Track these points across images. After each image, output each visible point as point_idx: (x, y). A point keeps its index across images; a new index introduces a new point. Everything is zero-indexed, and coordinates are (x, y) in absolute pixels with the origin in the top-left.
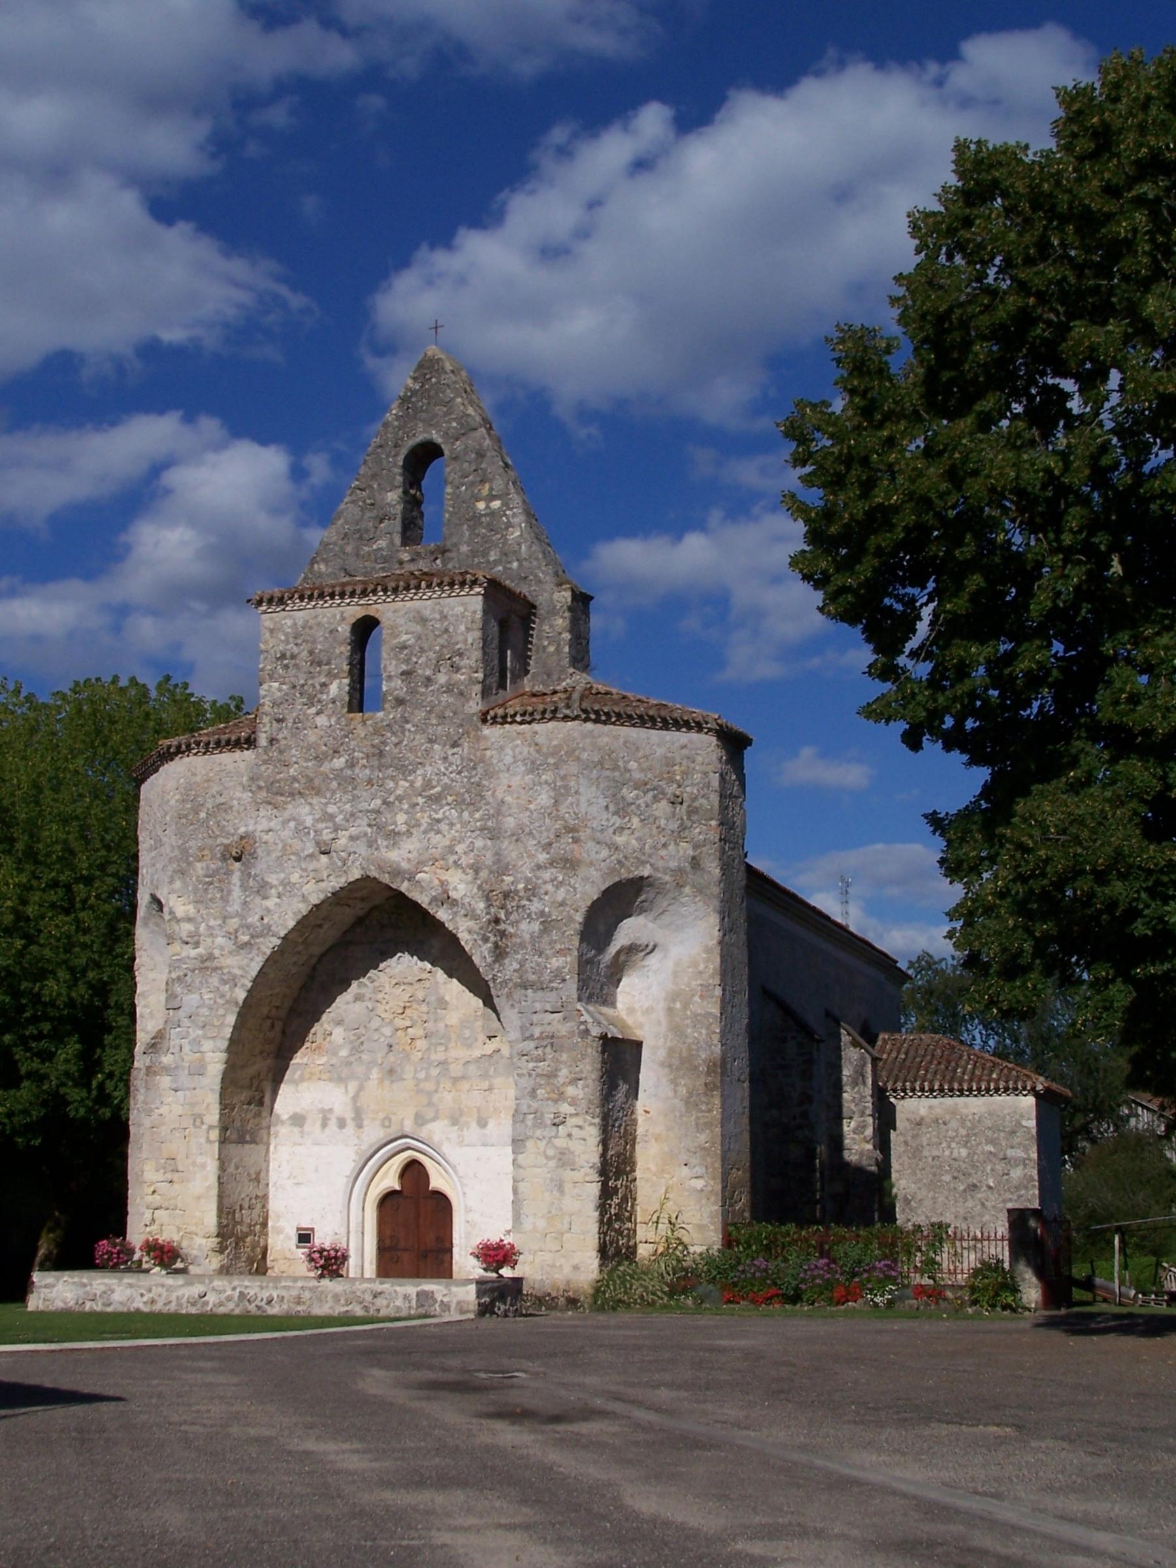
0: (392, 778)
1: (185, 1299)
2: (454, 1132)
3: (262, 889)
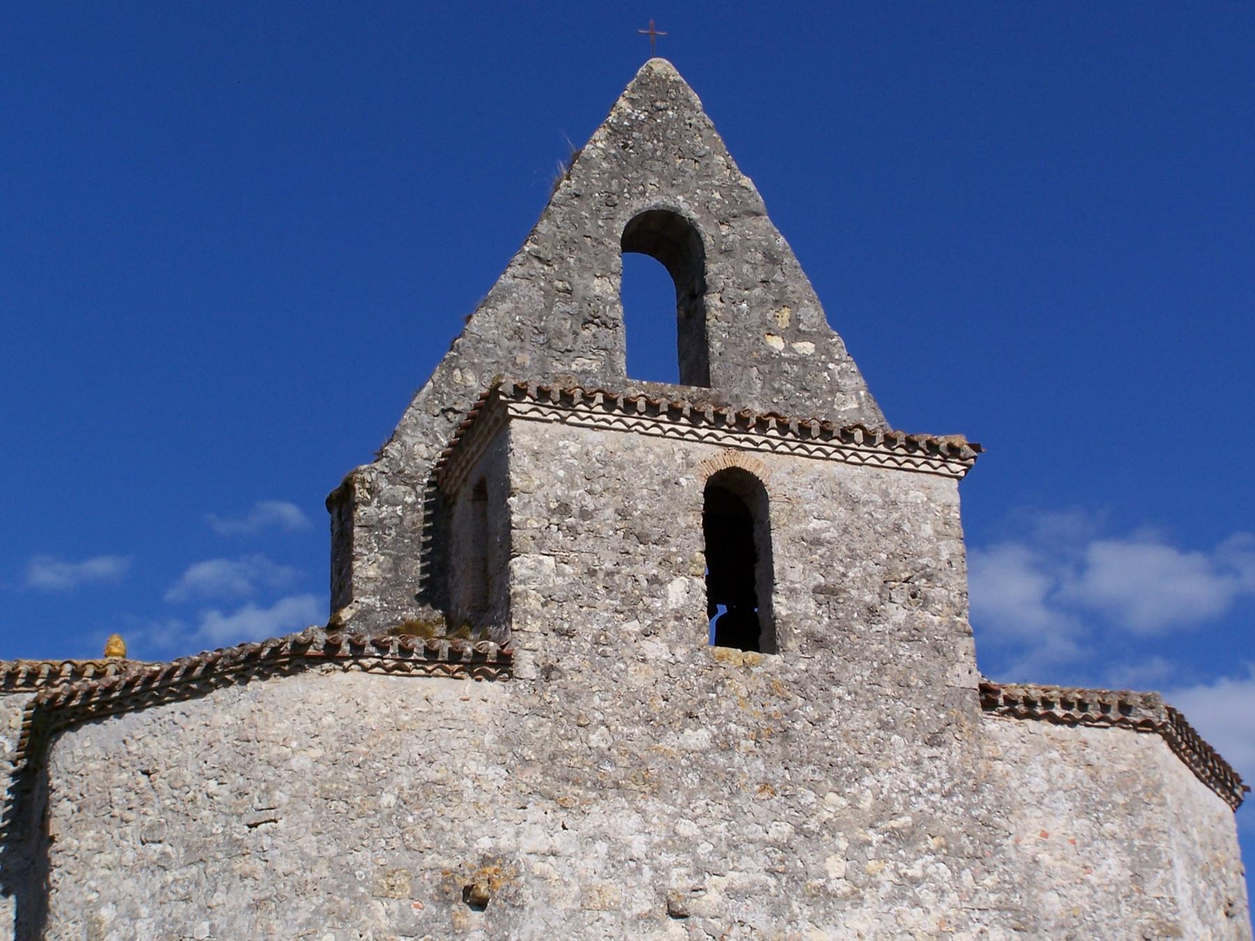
0: (813, 786)
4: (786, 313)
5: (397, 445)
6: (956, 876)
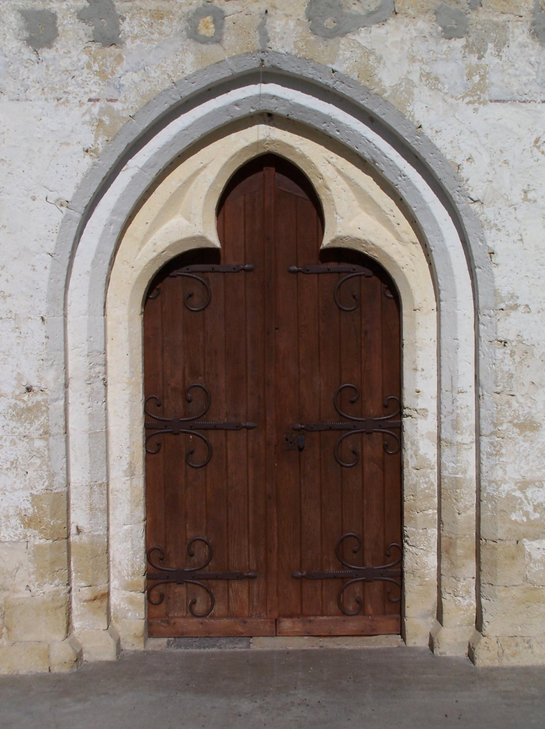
2: (451, 60)
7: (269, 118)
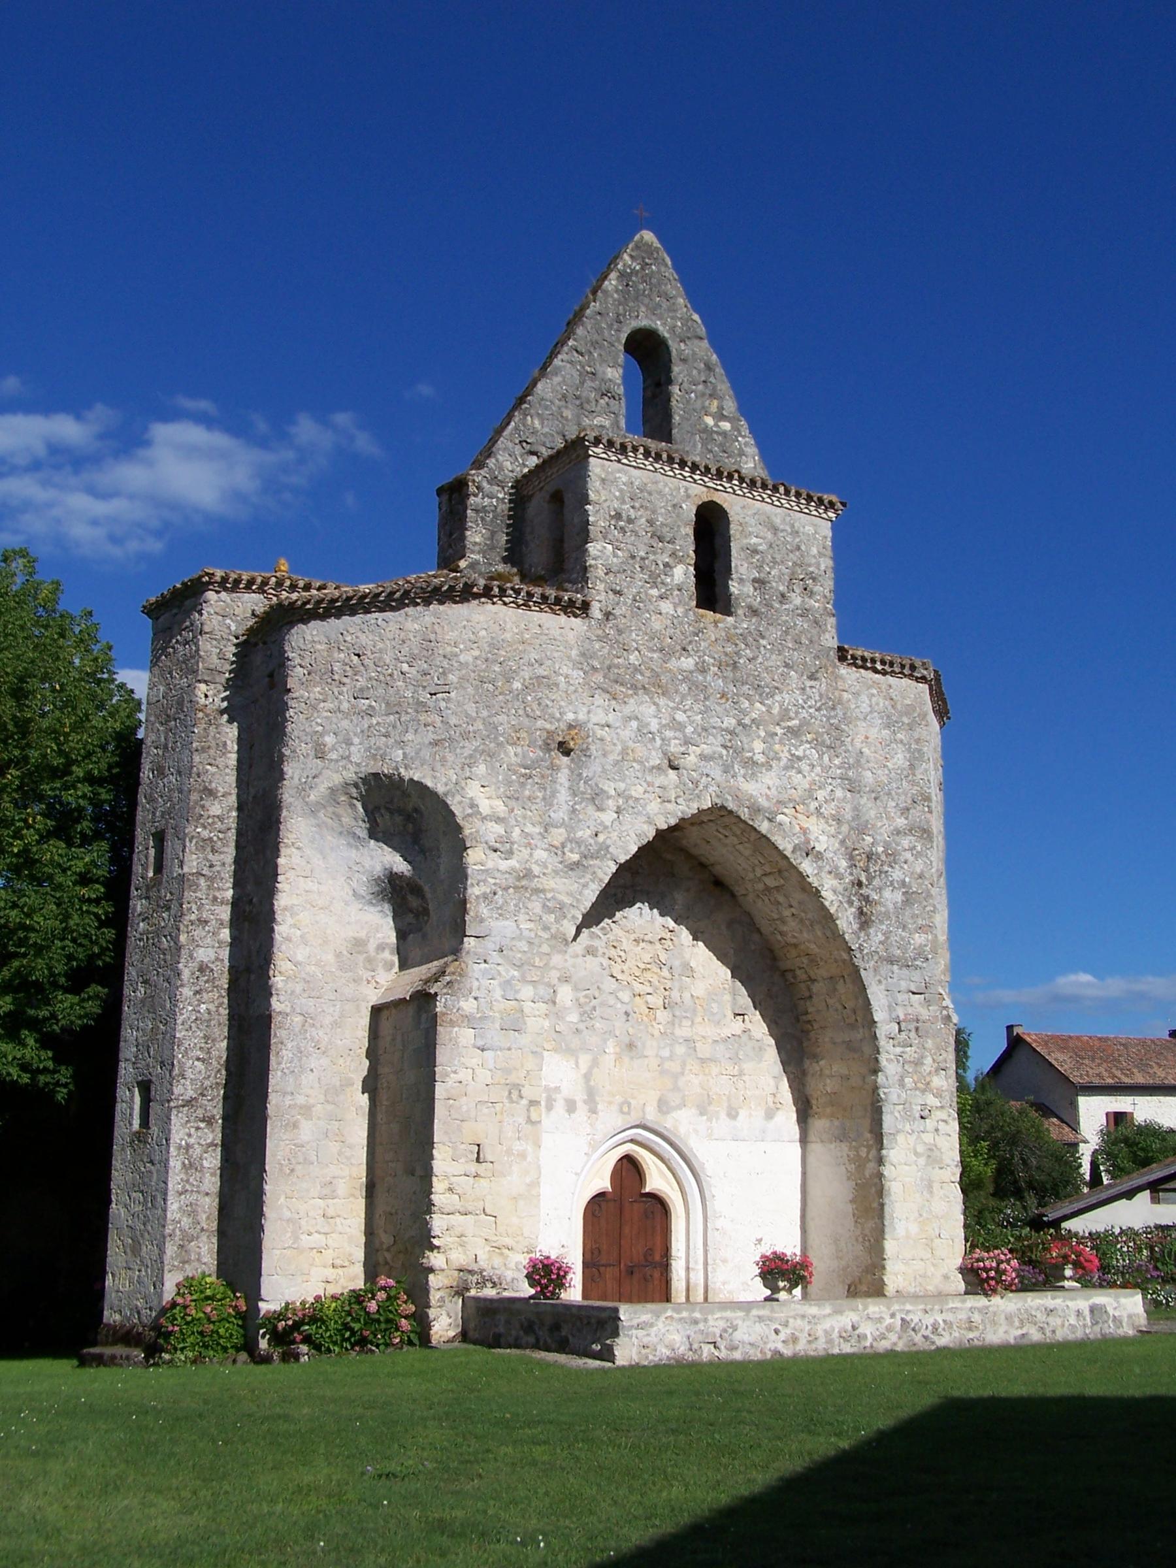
0: (748, 697)
1: (835, 1335)
3: (596, 798)
4: (715, 403)
5: (493, 460)
6: (821, 757)
7: (632, 1141)
